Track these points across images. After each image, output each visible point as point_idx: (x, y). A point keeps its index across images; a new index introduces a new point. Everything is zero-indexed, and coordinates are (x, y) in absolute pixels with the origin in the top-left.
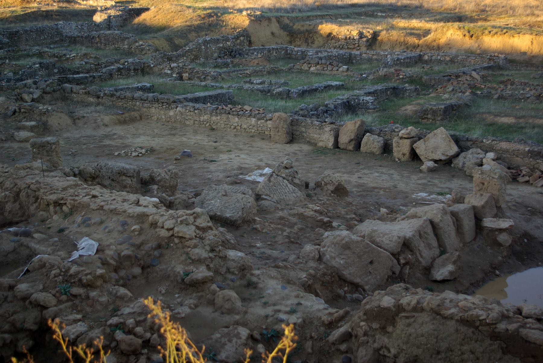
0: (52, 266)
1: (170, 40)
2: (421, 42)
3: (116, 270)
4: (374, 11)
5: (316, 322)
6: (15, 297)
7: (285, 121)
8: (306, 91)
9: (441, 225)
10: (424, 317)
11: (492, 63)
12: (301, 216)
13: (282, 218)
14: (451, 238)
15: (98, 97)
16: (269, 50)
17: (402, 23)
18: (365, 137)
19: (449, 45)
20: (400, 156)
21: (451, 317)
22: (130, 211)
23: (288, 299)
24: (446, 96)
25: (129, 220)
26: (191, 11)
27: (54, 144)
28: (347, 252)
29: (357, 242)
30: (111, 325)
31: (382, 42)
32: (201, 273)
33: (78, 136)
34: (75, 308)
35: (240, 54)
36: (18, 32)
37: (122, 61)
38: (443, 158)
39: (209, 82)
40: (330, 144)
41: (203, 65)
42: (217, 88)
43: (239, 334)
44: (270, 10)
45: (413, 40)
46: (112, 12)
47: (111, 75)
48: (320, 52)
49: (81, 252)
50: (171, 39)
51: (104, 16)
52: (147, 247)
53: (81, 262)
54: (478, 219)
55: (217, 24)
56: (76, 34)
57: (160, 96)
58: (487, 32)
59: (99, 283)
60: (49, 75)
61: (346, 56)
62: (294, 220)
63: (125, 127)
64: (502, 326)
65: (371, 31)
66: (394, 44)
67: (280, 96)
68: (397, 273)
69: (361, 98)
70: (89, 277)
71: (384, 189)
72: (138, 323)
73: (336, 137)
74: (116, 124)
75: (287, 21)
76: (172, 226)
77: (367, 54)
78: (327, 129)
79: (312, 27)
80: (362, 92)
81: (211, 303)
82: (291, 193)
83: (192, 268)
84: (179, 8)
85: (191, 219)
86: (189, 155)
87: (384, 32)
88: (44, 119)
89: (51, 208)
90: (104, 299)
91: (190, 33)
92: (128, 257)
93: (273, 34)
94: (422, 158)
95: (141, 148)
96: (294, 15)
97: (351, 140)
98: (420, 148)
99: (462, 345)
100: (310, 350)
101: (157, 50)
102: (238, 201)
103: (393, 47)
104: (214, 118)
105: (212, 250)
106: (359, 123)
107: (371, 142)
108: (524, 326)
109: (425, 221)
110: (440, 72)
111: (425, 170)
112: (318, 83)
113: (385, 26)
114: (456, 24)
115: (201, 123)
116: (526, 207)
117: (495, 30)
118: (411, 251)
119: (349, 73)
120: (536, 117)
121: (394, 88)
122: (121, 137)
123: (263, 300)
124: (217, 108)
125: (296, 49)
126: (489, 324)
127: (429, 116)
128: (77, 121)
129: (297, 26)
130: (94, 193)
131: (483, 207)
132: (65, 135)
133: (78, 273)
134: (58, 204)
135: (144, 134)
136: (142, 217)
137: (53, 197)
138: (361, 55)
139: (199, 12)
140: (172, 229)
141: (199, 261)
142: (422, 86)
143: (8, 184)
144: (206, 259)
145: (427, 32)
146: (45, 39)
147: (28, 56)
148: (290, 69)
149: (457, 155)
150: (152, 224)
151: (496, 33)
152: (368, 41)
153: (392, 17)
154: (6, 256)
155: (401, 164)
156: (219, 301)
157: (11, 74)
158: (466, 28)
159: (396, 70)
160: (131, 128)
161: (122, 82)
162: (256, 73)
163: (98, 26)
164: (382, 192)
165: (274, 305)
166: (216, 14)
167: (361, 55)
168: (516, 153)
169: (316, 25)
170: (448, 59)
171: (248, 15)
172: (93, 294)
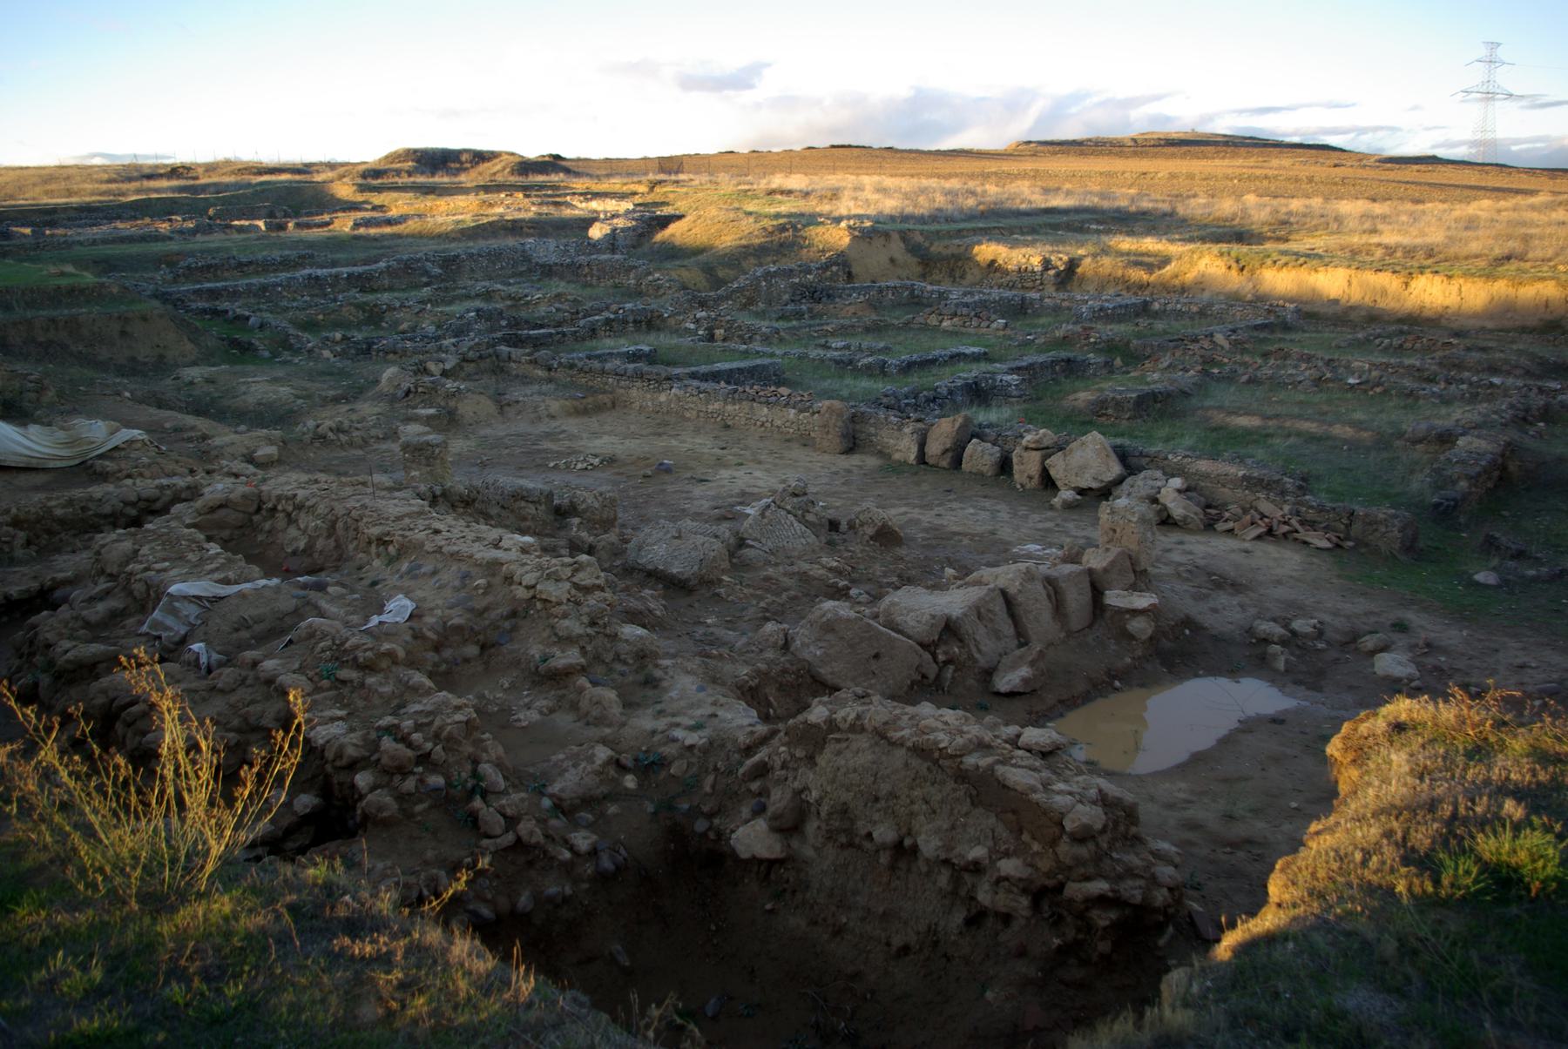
0: (324, 636)
1: (708, 270)
2: (1152, 278)
3: (437, 648)
4: (1083, 222)
5: (729, 746)
6: (257, 678)
7: (840, 415)
8: (915, 363)
9: (1020, 599)
10: (862, 741)
11: (1272, 318)
12: (804, 577)
13: (768, 579)
14: (1041, 621)
15: (550, 370)
16: (880, 290)
17: (1126, 243)
18: (970, 446)
19: (1200, 284)
20: (1025, 480)
21: (900, 744)
22: (478, 556)
23: (699, 707)
24: (1156, 376)
25: (474, 571)
26: (751, 220)
27: (437, 446)
28: (829, 637)
29: (848, 620)
30: (379, 729)
31: (1082, 279)
32: (569, 657)
33: (502, 434)
34: (339, 701)
35: (829, 296)
36: (457, 256)
37: (614, 307)
38: (1094, 485)
39: (756, 346)
40: (912, 457)
41: (761, 315)
42: (765, 354)
43: (594, 755)
44: (892, 218)
45: (1138, 275)
46: (620, 223)
47: (594, 330)
48: (971, 293)
49: (383, 618)
50: (712, 269)
51: (607, 229)
52: (494, 614)
53: (383, 633)
54: (1097, 592)
55: (793, 244)
56: (554, 259)
57: (646, 368)
58: (1269, 262)
59: (384, 664)
60: (492, 330)
61: (1017, 301)
62: (787, 581)
63: (585, 420)
64: (970, 760)
65: (1065, 258)
66: (1104, 283)
67: (868, 371)
68: (932, 676)
69: (999, 377)
70: (369, 654)
71: (972, 536)
72: (418, 727)
73: (922, 445)
74: (569, 414)
75: (919, 239)
76: (533, 582)
77: (1052, 296)
78: (907, 430)
79: (962, 249)
80: (1005, 367)
81: (574, 707)
82: (796, 536)
83: (556, 651)
84: (732, 215)
85: (568, 571)
86: (668, 470)
87: (1088, 260)
88: (452, 403)
89: (373, 548)
90: (386, 689)
91: (745, 258)
92: (458, 629)
93: (892, 260)
94: (1059, 483)
95: (596, 456)
96: (934, 227)
97: (946, 451)
98: (1057, 467)
99: (912, 788)
100: (708, 789)
101: (685, 288)
102: (695, 548)
103: (1102, 287)
104: (729, 408)
105: (593, 624)
106: (960, 420)
107: (980, 455)
108: (1004, 761)
109: (993, 590)
110: (1165, 332)
111: (1058, 506)
112: (941, 348)
113: (1090, 248)
114: (1216, 248)
115: (710, 415)
116: (1210, 574)
117: (1284, 259)
118: (961, 641)
119: (1008, 332)
120: (1300, 417)
121: (1069, 361)
122: (572, 437)
123: (658, 707)
124: (736, 391)
125: (929, 288)
126: (952, 757)
127: (1110, 411)
128: (507, 409)
129: (937, 248)
130: (437, 525)
131: (1105, 570)
132: (482, 432)
133: (357, 647)
134: (382, 541)
135: (609, 433)
136: (493, 566)
137: (375, 531)
138: (1041, 299)
139: (767, 223)
140: (533, 587)
141: (567, 640)
142: (1126, 355)
143: (322, 509)
144: (580, 636)
145: (1166, 261)
146: (502, 268)
147: (468, 297)
148: (907, 324)
149: (1119, 481)
150: (506, 578)
151: (1286, 264)
152: (1058, 275)
153: (1108, 232)
154: (281, 619)
155: (1025, 495)
156: (584, 704)
157: (432, 328)
158: (1233, 254)
159: (1085, 329)
160: (593, 422)
161: (607, 344)
162: (843, 331)
163: (594, 246)
164: (966, 541)
165: (674, 715)
166: (794, 227)
167: (1041, 299)
168: (1222, 480)
169: (970, 247)
170: (1195, 309)
171: (849, 227)
172: (371, 680)
